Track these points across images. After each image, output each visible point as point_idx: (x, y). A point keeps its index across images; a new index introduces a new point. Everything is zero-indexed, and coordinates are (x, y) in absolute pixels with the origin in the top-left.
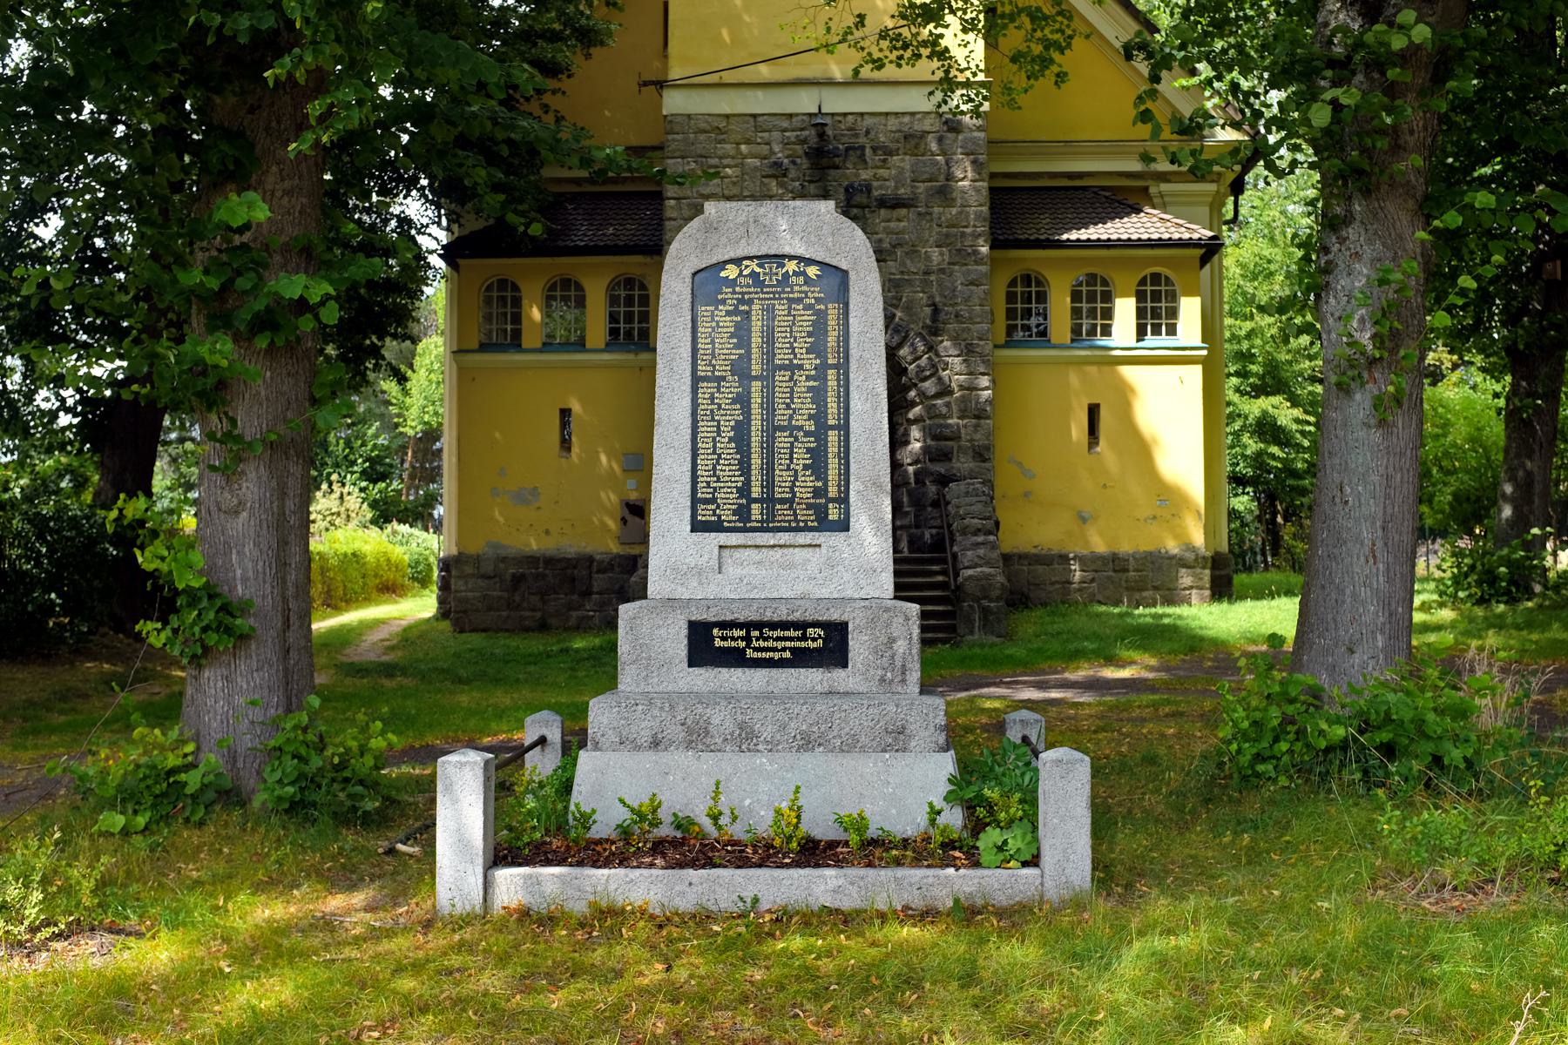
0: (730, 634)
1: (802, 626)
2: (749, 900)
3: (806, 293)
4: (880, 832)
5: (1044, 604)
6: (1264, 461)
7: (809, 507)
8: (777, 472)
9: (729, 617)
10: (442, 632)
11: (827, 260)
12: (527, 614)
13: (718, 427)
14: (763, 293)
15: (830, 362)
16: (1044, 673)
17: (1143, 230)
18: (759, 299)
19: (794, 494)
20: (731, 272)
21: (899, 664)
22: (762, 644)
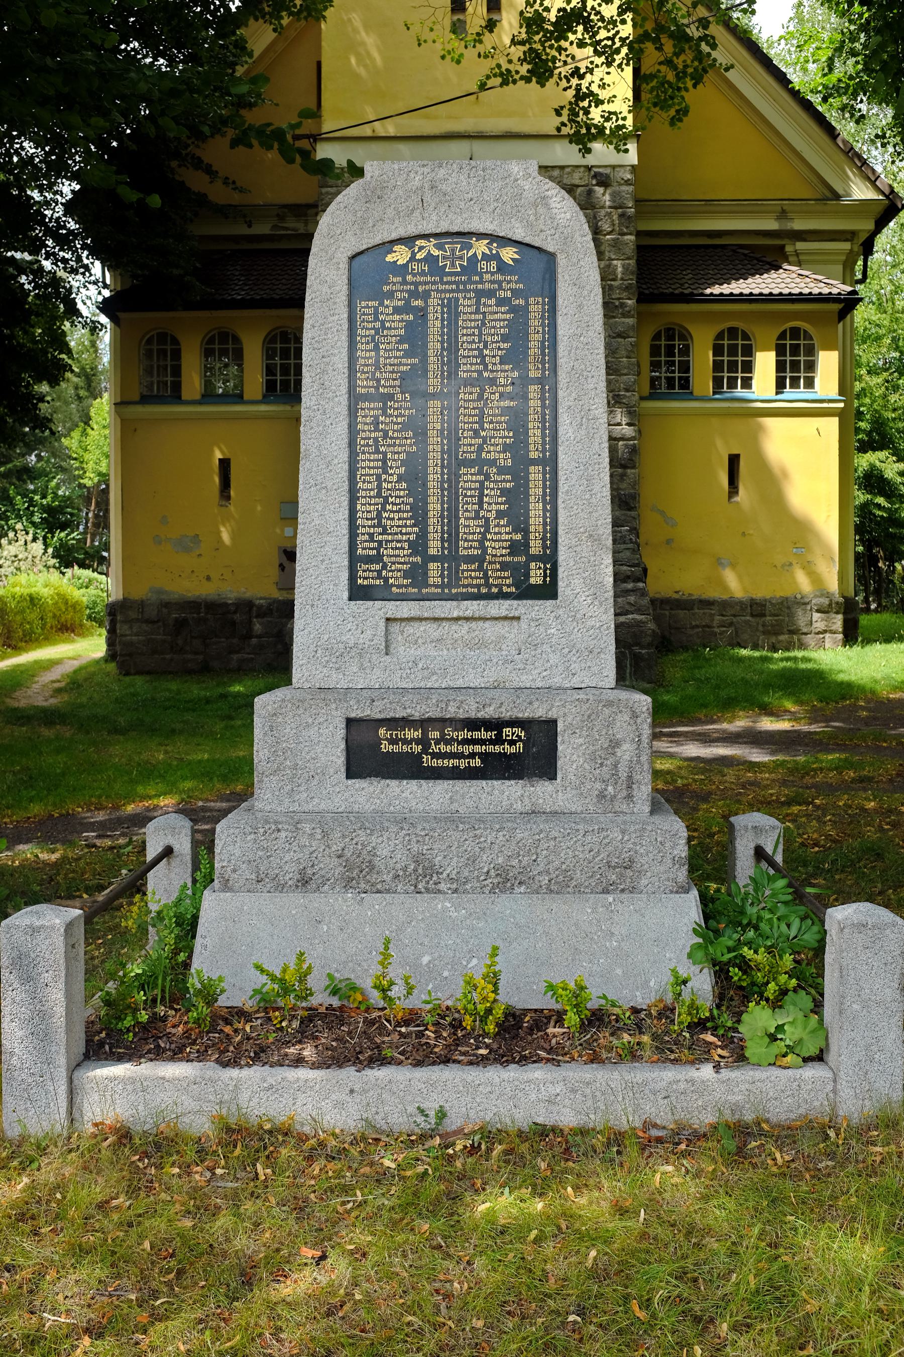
0: (401, 735)
1: (496, 725)
2: (432, 1114)
3: (500, 283)
4: (603, 1002)
5: (686, 648)
6: (871, 513)
7: (504, 566)
8: (462, 521)
9: (400, 714)
10: (108, 674)
11: (527, 240)
12: (189, 656)
13: (384, 461)
14: (443, 283)
15: (532, 374)
16: (699, 722)
17: (783, 285)
18: (437, 291)
19: (484, 549)
20: (400, 255)
21: (623, 774)
22: (443, 748)
